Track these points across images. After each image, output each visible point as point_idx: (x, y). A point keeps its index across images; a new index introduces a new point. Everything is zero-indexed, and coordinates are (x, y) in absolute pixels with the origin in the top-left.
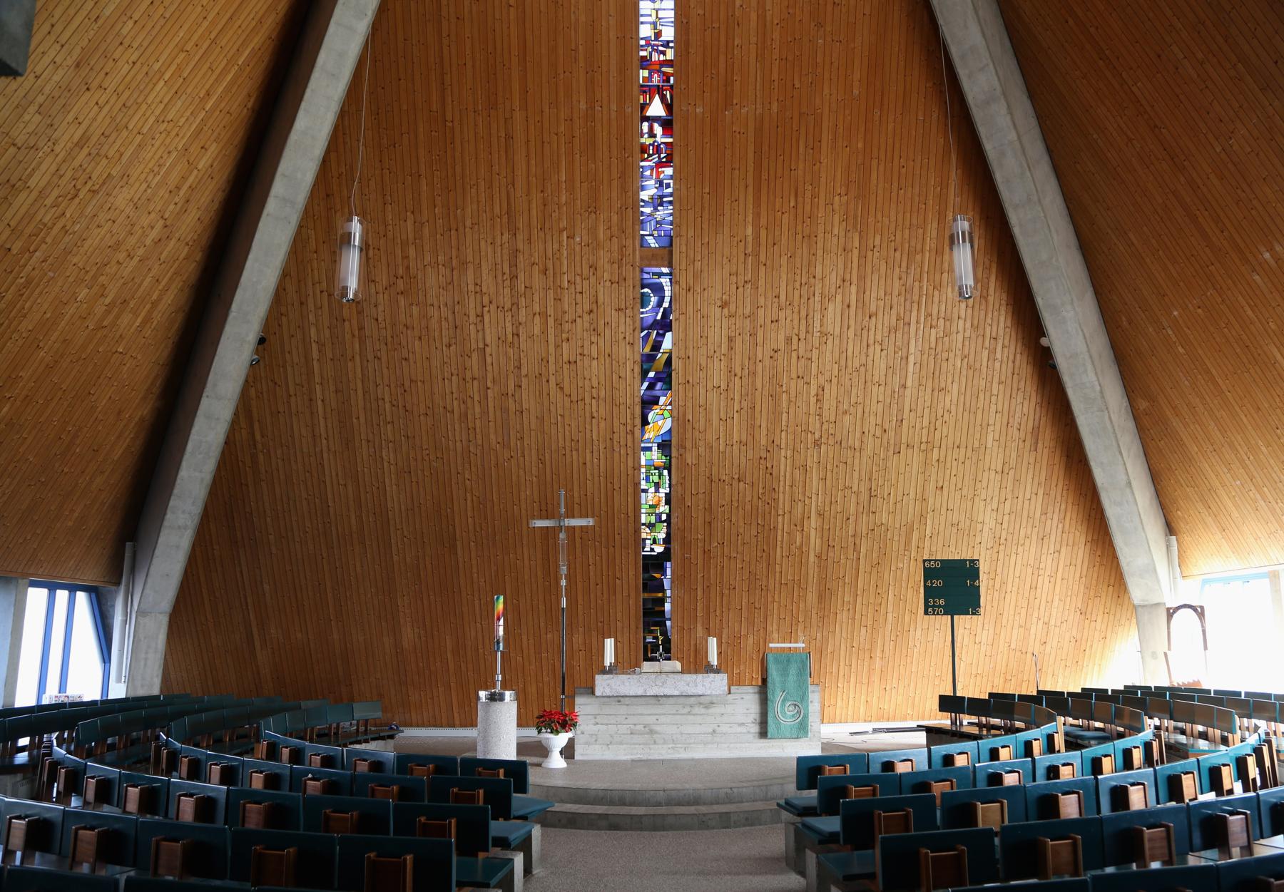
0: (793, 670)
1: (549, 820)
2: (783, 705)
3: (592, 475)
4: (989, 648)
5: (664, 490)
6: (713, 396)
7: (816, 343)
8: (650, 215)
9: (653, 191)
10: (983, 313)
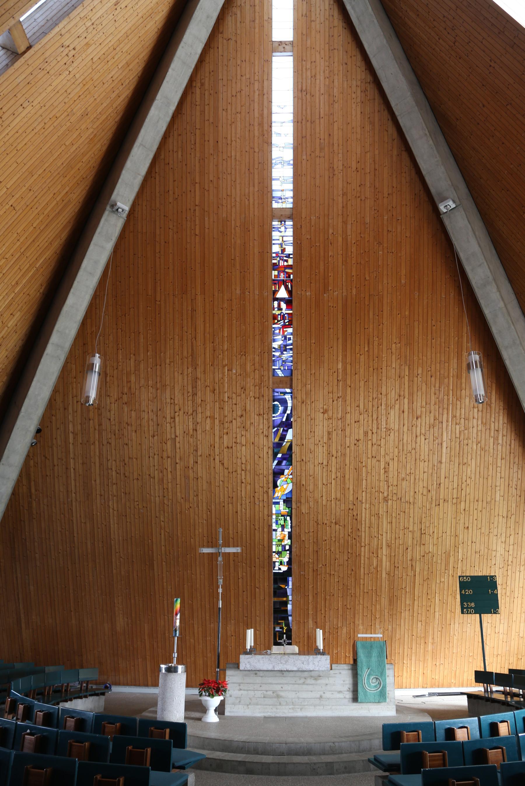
0: (375, 653)
1: (202, 765)
2: (368, 678)
3: (242, 519)
4: (505, 636)
5: (287, 530)
6: (318, 469)
7: (383, 435)
8: (279, 357)
9: (280, 342)
10: (488, 415)
